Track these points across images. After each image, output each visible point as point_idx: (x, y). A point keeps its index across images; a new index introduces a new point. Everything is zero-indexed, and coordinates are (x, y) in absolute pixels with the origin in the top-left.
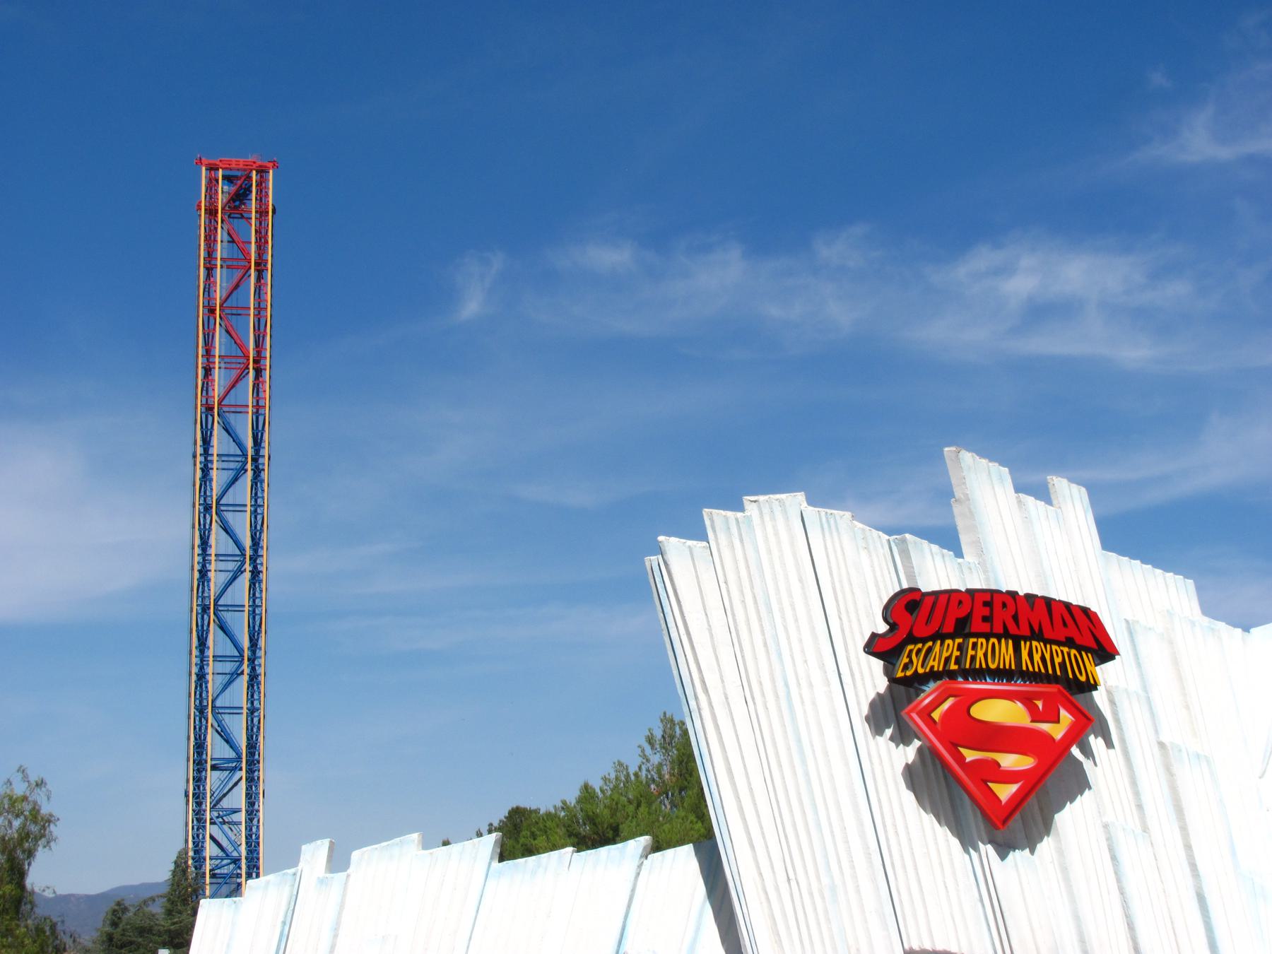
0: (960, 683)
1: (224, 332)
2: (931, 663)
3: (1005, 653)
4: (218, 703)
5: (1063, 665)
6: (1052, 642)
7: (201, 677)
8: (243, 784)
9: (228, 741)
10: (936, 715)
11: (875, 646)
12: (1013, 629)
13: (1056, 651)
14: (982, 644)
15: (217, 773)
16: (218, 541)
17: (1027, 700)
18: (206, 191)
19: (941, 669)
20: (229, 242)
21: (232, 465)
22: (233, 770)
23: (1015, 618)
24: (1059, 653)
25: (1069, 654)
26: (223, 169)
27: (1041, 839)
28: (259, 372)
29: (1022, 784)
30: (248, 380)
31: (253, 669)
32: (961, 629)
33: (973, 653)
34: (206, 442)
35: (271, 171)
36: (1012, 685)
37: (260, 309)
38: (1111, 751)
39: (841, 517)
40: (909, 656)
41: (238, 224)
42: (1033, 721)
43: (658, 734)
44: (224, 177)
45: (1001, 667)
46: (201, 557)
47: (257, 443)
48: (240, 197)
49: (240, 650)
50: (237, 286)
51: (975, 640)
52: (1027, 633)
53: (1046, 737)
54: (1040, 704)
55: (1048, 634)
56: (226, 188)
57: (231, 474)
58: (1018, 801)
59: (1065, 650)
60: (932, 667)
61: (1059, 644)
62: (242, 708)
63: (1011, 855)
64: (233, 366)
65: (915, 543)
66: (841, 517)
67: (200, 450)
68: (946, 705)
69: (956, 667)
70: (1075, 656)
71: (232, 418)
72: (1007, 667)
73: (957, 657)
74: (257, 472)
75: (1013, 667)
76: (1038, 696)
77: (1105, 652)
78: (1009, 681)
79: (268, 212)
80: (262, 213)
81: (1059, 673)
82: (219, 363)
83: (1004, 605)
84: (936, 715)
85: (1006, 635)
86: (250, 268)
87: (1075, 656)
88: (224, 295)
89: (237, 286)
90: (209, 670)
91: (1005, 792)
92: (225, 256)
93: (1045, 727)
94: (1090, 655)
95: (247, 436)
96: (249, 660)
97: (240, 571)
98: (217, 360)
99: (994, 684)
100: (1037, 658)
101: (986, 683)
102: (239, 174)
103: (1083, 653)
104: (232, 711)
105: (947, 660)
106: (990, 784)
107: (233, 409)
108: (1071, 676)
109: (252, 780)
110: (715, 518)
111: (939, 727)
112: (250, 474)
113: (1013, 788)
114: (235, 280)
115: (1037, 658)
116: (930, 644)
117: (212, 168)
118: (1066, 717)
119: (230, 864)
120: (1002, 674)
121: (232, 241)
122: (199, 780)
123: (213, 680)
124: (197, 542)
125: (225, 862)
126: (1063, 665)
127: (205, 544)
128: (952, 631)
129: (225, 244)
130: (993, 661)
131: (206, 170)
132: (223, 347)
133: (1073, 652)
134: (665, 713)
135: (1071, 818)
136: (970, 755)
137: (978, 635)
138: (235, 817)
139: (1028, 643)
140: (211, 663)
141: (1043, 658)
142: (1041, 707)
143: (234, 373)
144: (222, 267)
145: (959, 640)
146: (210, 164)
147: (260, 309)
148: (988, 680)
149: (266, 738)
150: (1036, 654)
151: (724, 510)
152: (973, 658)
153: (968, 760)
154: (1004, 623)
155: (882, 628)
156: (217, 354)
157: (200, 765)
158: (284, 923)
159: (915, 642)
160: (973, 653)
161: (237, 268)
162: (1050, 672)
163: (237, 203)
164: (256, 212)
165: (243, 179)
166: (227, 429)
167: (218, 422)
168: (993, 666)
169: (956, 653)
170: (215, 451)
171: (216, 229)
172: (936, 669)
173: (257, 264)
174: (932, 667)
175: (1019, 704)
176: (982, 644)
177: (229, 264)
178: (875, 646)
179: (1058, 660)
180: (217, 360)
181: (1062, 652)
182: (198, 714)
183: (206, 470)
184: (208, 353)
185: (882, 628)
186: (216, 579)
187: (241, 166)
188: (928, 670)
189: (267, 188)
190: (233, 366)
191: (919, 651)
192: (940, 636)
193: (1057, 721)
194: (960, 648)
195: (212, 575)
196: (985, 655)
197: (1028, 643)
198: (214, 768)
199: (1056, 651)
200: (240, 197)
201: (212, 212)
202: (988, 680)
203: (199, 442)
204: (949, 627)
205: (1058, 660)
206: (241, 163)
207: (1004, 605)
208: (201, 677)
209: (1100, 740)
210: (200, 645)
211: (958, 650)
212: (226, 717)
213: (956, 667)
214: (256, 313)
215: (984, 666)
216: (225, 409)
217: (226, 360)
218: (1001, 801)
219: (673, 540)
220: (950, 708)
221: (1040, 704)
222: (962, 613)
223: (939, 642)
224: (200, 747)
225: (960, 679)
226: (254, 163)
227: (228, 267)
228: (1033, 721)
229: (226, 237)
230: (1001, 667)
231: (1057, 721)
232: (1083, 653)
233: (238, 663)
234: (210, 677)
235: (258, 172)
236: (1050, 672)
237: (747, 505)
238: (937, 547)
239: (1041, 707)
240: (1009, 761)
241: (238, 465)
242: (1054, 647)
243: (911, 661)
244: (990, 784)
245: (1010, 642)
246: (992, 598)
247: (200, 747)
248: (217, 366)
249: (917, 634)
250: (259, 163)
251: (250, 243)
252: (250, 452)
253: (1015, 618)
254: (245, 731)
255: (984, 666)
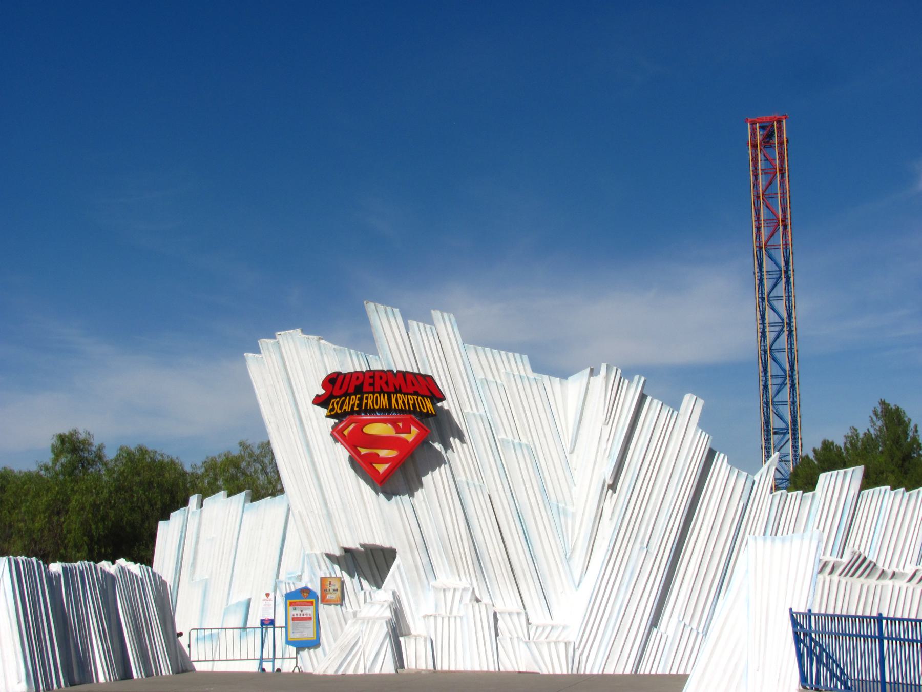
0: (363, 416)
1: (765, 207)
2: (344, 407)
3: (384, 401)
4: (775, 400)
5: (414, 405)
6: (408, 394)
7: (766, 387)
8: (790, 442)
9: (781, 418)
10: (346, 432)
11: (320, 401)
12: (385, 388)
13: (411, 398)
14: (371, 397)
15: (776, 436)
16: (770, 316)
17: (394, 423)
18: (751, 135)
19: (349, 410)
20: (765, 160)
21: (775, 276)
22: (784, 434)
23: (387, 383)
24: (412, 399)
25: (417, 399)
26: (758, 122)
27: (417, 490)
28: (785, 227)
29: (391, 465)
30: (779, 232)
31: (793, 381)
32: (359, 390)
33: (366, 401)
34: (760, 265)
35: (784, 121)
36: (390, 416)
37: (783, 194)
38: (465, 445)
39: (313, 339)
40: (333, 404)
41: (768, 150)
42: (396, 433)
43: (879, 410)
44: (759, 127)
45: (381, 407)
46: (792, 321)
47: (787, 263)
48: (769, 136)
49: (784, 370)
50: (770, 183)
51: (367, 395)
52: (393, 390)
53: (405, 441)
54: (400, 425)
55: (403, 390)
56: (761, 132)
57: (774, 281)
58: (388, 473)
59: (415, 397)
60: (345, 410)
61: (412, 394)
62: (787, 402)
63: (394, 498)
64: (772, 225)
65: (340, 349)
66: (313, 339)
67: (757, 270)
68: (351, 428)
69: (357, 409)
70: (421, 400)
71: (773, 252)
72: (384, 407)
73: (358, 404)
74: (788, 279)
75: (388, 407)
76: (399, 420)
77: (437, 396)
78: (388, 414)
79: (784, 143)
80: (781, 143)
81: (412, 408)
82: (764, 224)
83: (381, 378)
84: (346, 432)
85: (381, 392)
86: (777, 173)
87: (421, 400)
88: (764, 188)
89: (770, 183)
90: (769, 383)
91: (382, 468)
92: (763, 168)
93: (403, 436)
94: (428, 399)
95: (781, 260)
96: (789, 376)
97: (782, 331)
98: (762, 222)
99: (381, 416)
100: (400, 402)
101: (377, 416)
102: (768, 124)
103: (425, 399)
104: (783, 403)
105: (353, 406)
106: (374, 465)
107: (773, 247)
108: (418, 410)
109: (795, 439)
110: (264, 343)
111: (347, 438)
112: (784, 280)
113: (386, 466)
114: (769, 179)
115: (400, 402)
116: (344, 398)
117: (753, 123)
118: (415, 431)
119: (786, 481)
120: (382, 411)
121: (766, 160)
122: (768, 440)
123: (771, 388)
124: (759, 317)
125: (784, 481)
126: (414, 405)
127: (763, 318)
128: (353, 392)
129: (763, 162)
130: (377, 404)
131: (750, 124)
132: (765, 215)
133: (420, 398)
134: (881, 400)
135: (434, 480)
136: (363, 451)
137: (368, 393)
138: (787, 458)
139: (395, 395)
140: (770, 379)
141: (403, 402)
142: (401, 426)
143: (772, 228)
144: (762, 174)
145: (359, 396)
146: (752, 121)
147: (783, 194)
148: (377, 414)
149: (802, 417)
150: (399, 400)
151: (268, 339)
152: (366, 404)
153: (362, 453)
154: (381, 386)
155: (322, 392)
156: (762, 219)
157: (767, 431)
158: (182, 532)
159: (335, 397)
160: (366, 401)
161: (770, 173)
162: (407, 408)
163: (768, 140)
164: (778, 143)
165: (770, 127)
166: (770, 257)
167: (765, 254)
168: (377, 407)
169: (357, 402)
170: (764, 270)
171: (758, 154)
172: (347, 410)
173: (780, 170)
174: (345, 410)
175: (389, 425)
176: (371, 397)
177: (765, 172)
178: (320, 401)
179: (411, 403)
180: (762, 222)
181: (414, 398)
182: (765, 406)
183: (761, 280)
184: (758, 219)
185: (322, 392)
186: (770, 337)
187: (768, 120)
188: (342, 411)
189: (782, 130)
190: (772, 225)
191: (337, 403)
192: (347, 394)
193: (410, 432)
194: (359, 399)
195: (767, 334)
196: (373, 402)
197: (395, 395)
198: (775, 433)
199: (411, 398)
200: (769, 136)
201: (754, 146)
202: (377, 414)
203: (756, 266)
204: (351, 390)
205: (411, 403)
206: (768, 119)
207: (381, 378)
208: (766, 387)
209: (457, 440)
210: (764, 370)
211: (358, 400)
212: (780, 407)
213: (357, 409)
214: (782, 195)
215: (372, 407)
216: (768, 247)
217: (768, 222)
218: (380, 473)
219: (250, 354)
220: (353, 429)
221: (400, 425)
222: (358, 383)
223: (348, 397)
224: (767, 423)
225: (363, 414)
226: (775, 117)
227: (765, 173)
228: (396, 433)
229: (763, 158)
230: (381, 407)
231: (410, 432)
232: (425, 399)
233: (784, 379)
234: (770, 387)
235: (777, 122)
236: (407, 408)
237: (278, 337)
238: (353, 350)
239: (401, 426)
240: (384, 453)
241: (778, 276)
242: (409, 396)
243: (334, 408)
244: (374, 465)
245: (386, 395)
246: (374, 373)
247: (767, 423)
248: (763, 225)
249: (334, 394)
250: (778, 117)
251: (776, 159)
252: (783, 268)
253: (387, 383)
254: (789, 413)
255: (372, 407)
